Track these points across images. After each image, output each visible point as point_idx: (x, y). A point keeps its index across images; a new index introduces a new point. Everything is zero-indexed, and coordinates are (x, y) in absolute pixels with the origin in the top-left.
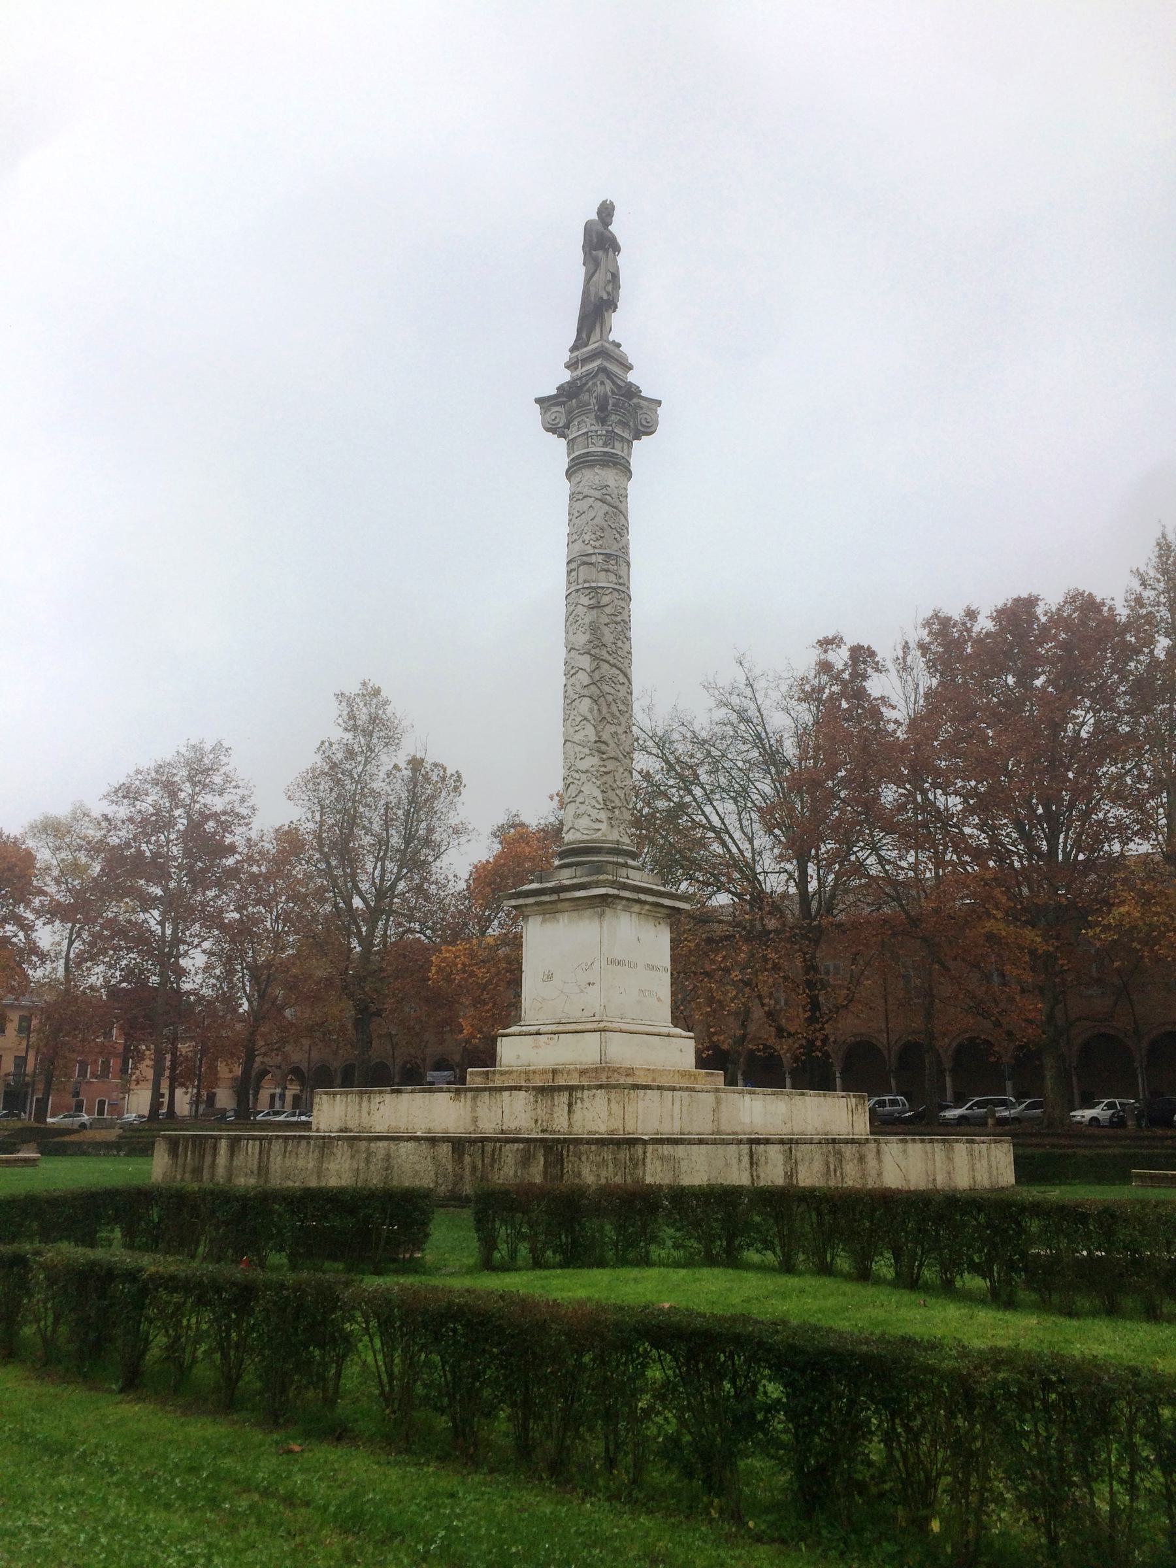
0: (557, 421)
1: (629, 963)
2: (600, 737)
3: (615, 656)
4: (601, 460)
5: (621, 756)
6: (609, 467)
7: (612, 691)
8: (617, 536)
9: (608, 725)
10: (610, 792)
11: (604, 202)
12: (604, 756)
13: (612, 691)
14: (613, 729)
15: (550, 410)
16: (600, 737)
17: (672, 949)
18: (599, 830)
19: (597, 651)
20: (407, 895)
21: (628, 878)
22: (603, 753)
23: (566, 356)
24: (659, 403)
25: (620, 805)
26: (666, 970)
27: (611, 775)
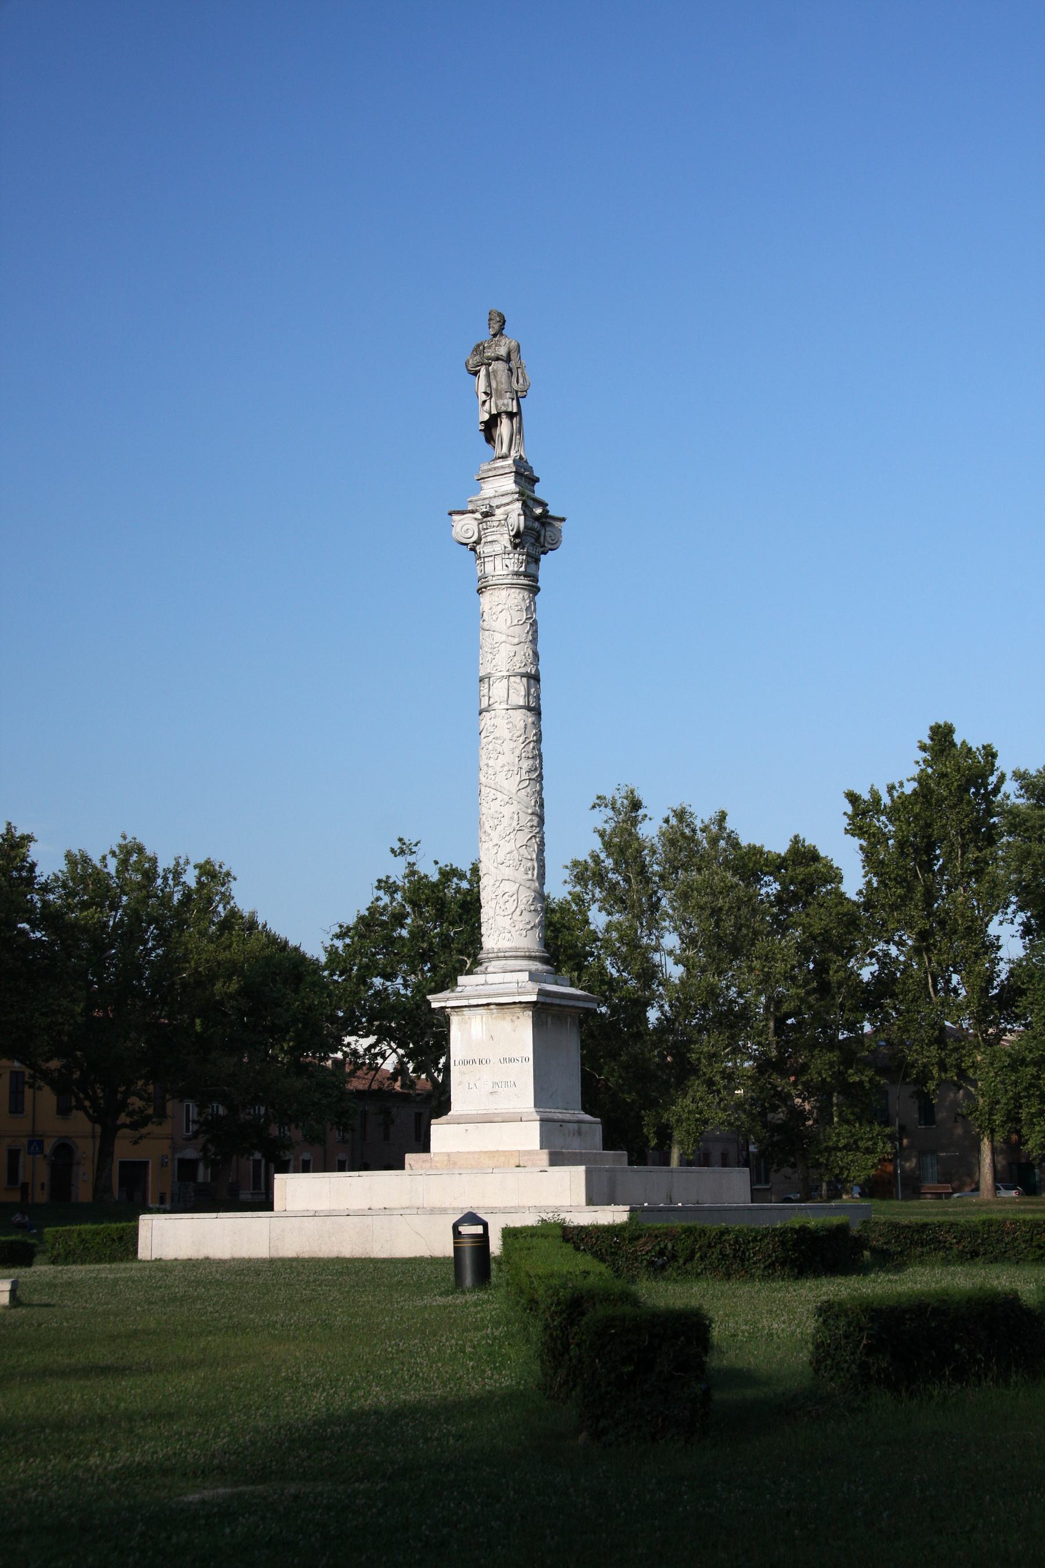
1: (481, 1062)
26: (527, 1060)
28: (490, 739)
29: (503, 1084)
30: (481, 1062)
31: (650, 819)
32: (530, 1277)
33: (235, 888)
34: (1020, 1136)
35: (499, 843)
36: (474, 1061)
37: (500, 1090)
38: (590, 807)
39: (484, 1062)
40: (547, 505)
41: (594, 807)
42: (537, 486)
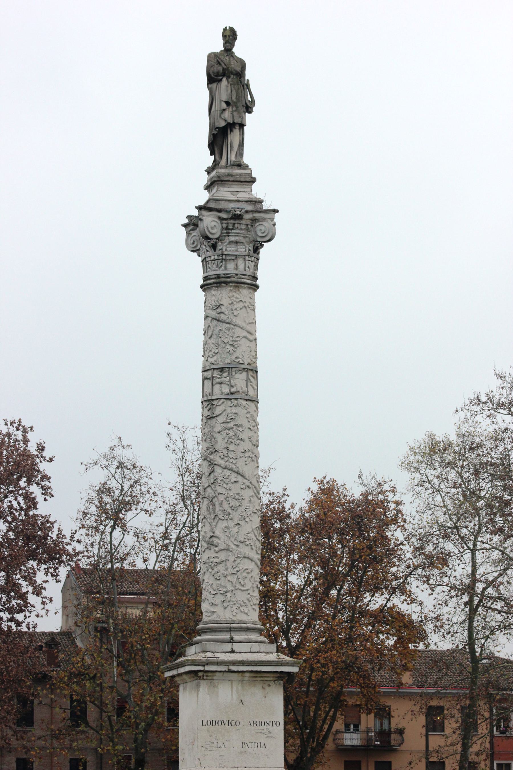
0: (196, 243)
1: (230, 723)
2: (214, 533)
3: (226, 459)
4: (214, 283)
5: (232, 546)
6: (223, 287)
7: (224, 491)
8: (231, 349)
9: (220, 521)
10: (222, 579)
11: (225, 30)
12: (217, 549)
13: (224, 491)
14: (225, 524)
15: (191, 234)
16: (214, 533)
17: (177, 739)
18: (214, 612)
19: (212, 457)
20: (477, 519)
21: (233, 651)
22: (216, 546)
23: (205, 179)
24: (275, 211)
25: (232, 588)
26: (277, 724)
27: (223, 564)
28: (231, 425)
29: (253, 745)
30: (230, 723)
31: (304, 499)
32: (20, 425)
33: (19, 620)
34: (30, 568)
35: (240, 523)
36: (222, 722)
37: (250, 750)
38: (499, 371)
39: (233, 723)
40: (261, 202)
41: (500, 377)
42: (254, 186)
